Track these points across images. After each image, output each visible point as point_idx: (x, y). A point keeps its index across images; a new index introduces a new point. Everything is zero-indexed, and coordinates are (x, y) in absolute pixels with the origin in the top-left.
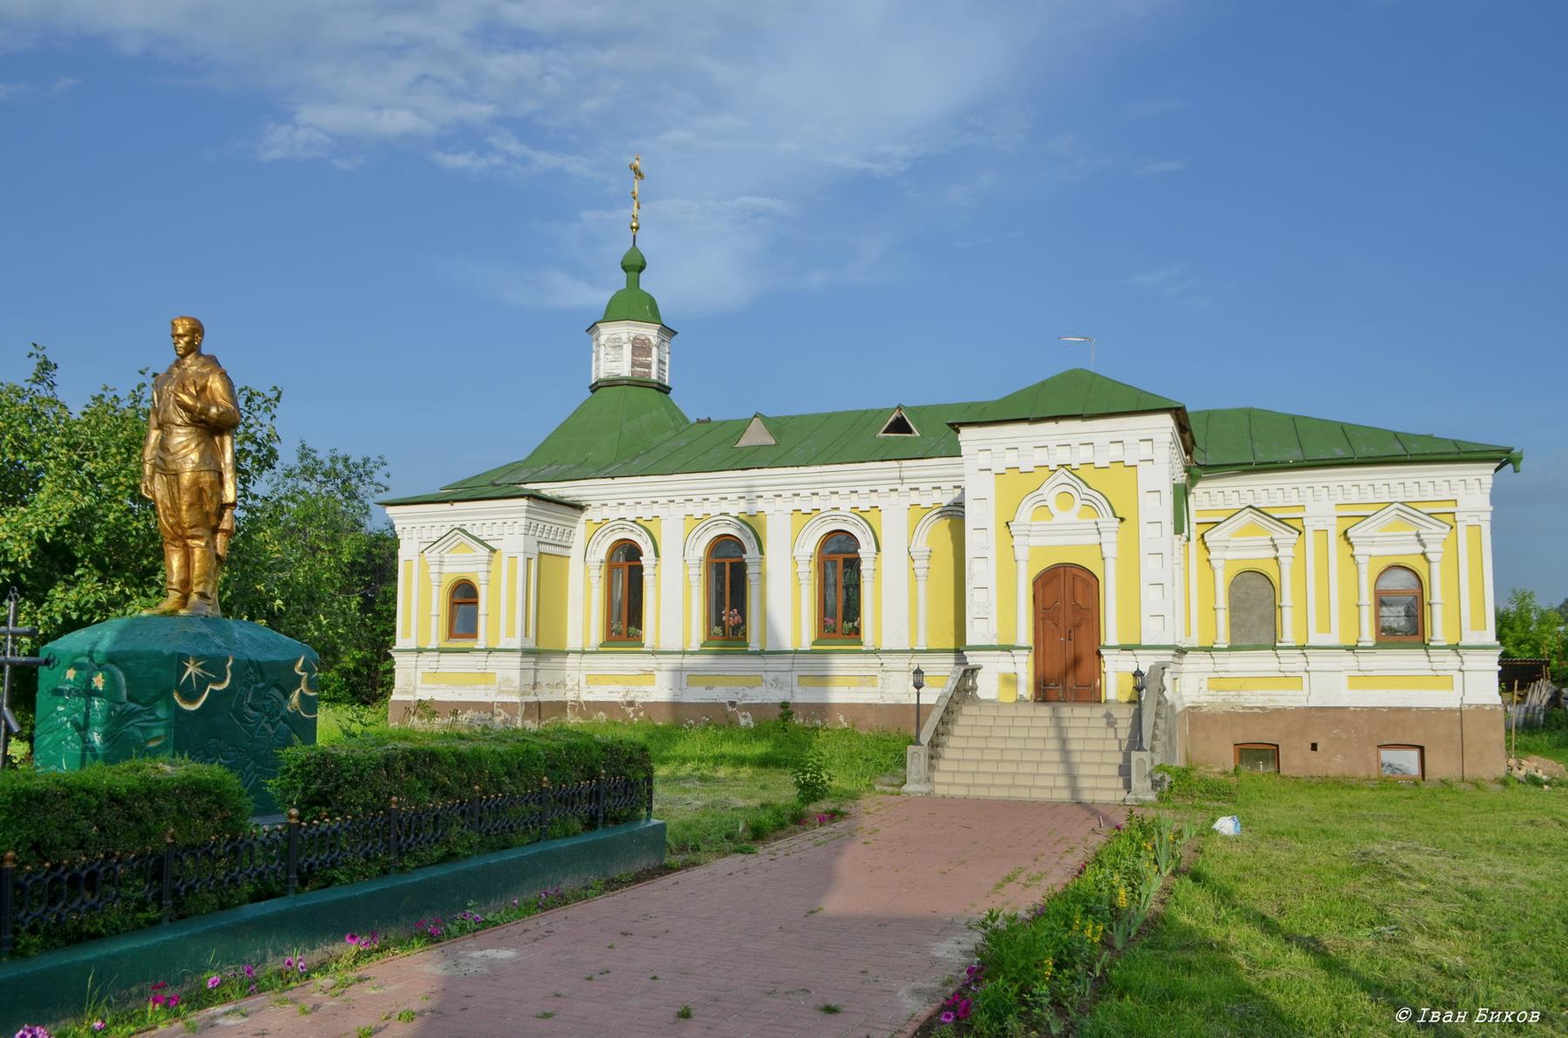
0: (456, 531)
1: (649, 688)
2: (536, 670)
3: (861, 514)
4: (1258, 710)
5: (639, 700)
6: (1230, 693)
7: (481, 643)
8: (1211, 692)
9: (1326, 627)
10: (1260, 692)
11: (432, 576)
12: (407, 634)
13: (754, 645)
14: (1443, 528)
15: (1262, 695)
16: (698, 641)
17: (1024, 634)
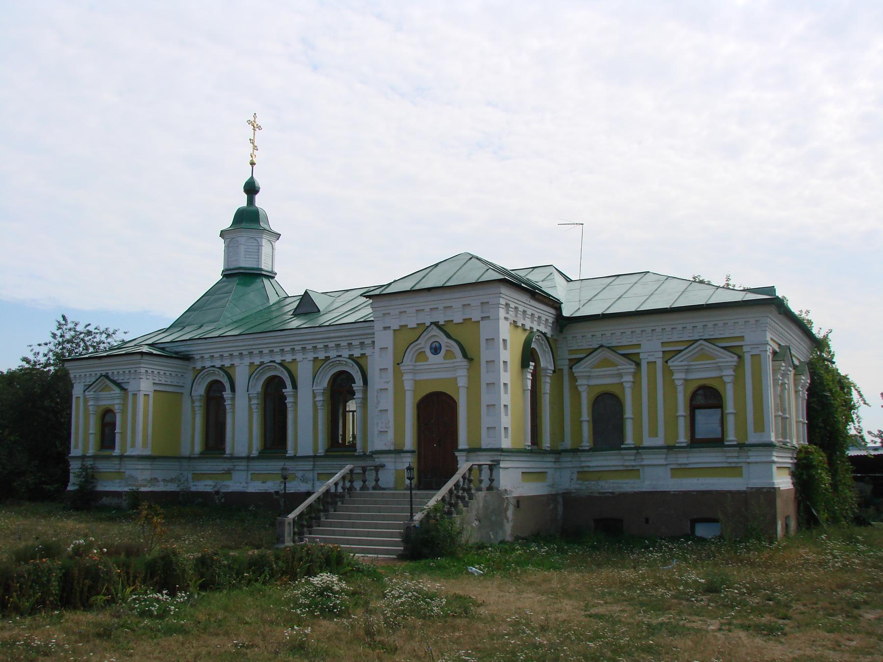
0: (102, 378)
1: (228, 483)
2: (248, 466)
3: (357, 361)
4: (608, 494)
5: (223, 490)
6: (593, 483)
7: (117, 452)
8: (580, 482)
9: (654, 433)
10: (612, 481)
11: (90, 407)
12: (76, 447)
13: (290, 452)
14: (733, 357)
15: (613, 483)
16: (257, 450)
17: (409, 441)
